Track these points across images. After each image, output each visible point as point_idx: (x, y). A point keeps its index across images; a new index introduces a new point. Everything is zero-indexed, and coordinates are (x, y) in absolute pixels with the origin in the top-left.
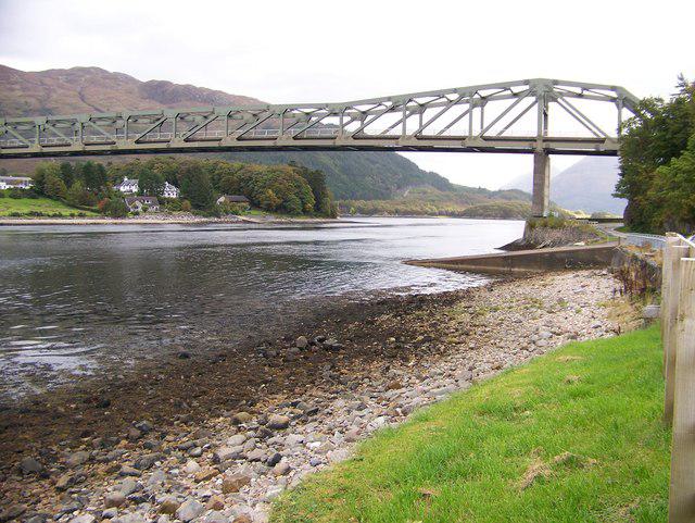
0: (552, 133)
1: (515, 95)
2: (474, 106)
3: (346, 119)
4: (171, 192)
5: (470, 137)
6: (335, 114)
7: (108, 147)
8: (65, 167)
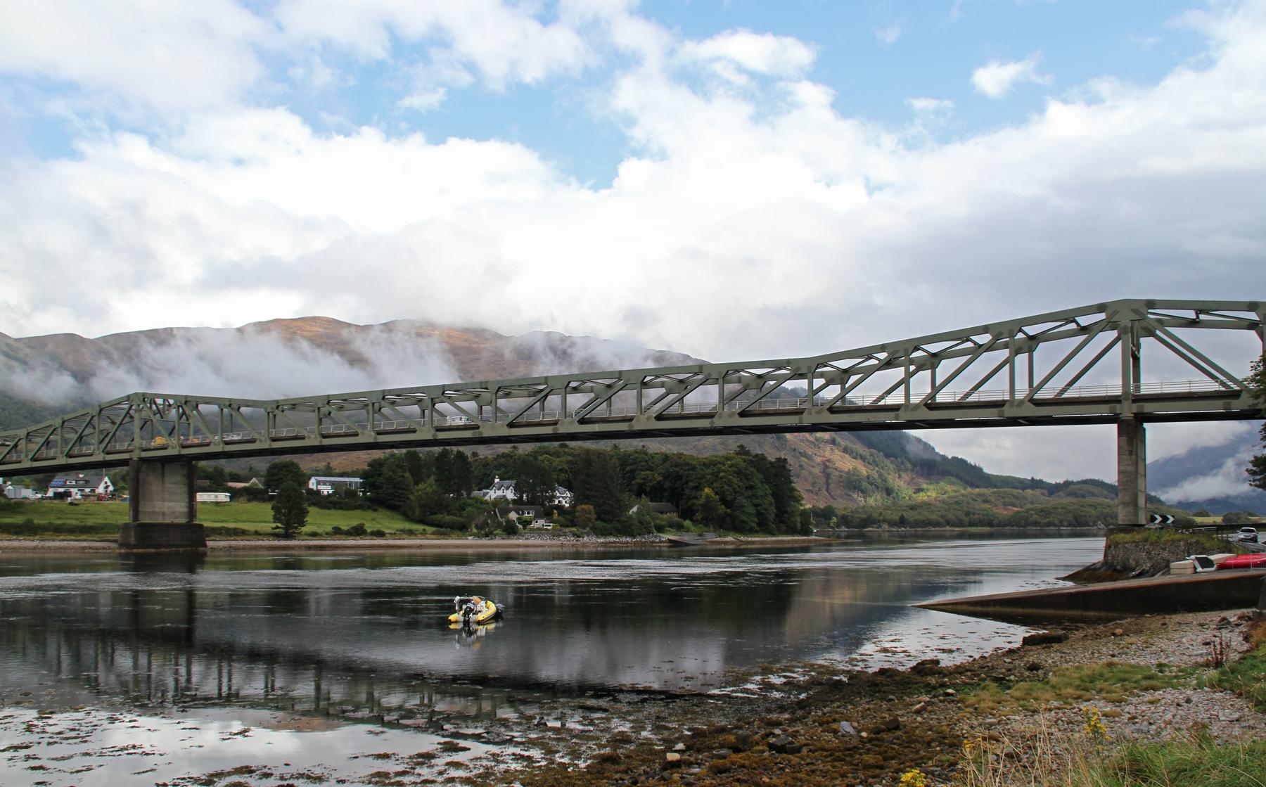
0: (1149, 384)
1: (1083, 330)
2: (1018, 351)
5: (1012, 402)
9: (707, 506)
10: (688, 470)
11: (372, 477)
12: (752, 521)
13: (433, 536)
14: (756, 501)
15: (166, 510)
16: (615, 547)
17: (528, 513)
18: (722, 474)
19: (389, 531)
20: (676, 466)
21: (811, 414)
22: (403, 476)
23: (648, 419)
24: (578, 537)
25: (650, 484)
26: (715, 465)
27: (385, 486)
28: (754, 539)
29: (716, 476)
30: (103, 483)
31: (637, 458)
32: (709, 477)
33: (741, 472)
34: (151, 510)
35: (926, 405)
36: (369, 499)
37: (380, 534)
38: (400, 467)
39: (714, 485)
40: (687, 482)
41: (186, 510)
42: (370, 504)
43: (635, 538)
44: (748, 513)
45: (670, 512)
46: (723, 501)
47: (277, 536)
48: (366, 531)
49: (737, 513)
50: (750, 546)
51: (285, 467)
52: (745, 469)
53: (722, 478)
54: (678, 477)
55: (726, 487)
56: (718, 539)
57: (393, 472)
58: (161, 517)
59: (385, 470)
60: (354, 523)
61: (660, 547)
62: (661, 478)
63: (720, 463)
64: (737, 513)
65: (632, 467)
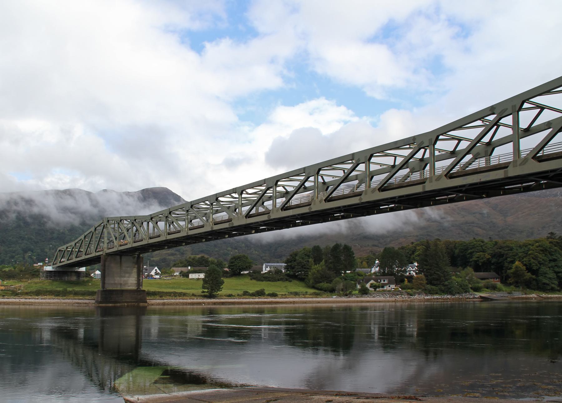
9: (517, 274)
10: (508, 250)
11: (291, 262)
12: (552, 283)
13: (311, 296)
14: (557, 269)
15: (122, 282)
16: (437, 302)
17: (384, 281)
18: (529, 252)
19: (281, 293)
20: (500, 249)
21: (432, 182)
22: (308, 261)
23: (320, 202)
24: (411, 295)
25: (482, 261)
26: (526, 246)
27: (296, 267)
28: (552, 296)
29: (526, 254)
30: (154, 270)
31: (475, 244)
32: (520, 254)
33: (546, 250)
34: (112, 282)
35: (534, 157)
36: (288, 275)
37: (274, 295)
38: (309, 256)
39: (524, 259)
40: (506, 259)
41: (136, 282)
42: (288, 278)
43: (454, 295)
44: (550, 278)
45: (494, 278)
46: (529, 269)
47: (205, 297)
48: (265, 293)
49: (540, 278)
50: (550, 300)
51: (239, 258)
52: (550, 248)
53: (530, 254)
54: (501, 255)
55: (532, 260)
56: (524, 296)
57: (303, 258)
58: (119, 286)
59: (297, 258)
60: (258, 289)
61: (474, 301)
62: (490, 257)
63: (530, 244)
64: (540, 278)
65: (472, 251)
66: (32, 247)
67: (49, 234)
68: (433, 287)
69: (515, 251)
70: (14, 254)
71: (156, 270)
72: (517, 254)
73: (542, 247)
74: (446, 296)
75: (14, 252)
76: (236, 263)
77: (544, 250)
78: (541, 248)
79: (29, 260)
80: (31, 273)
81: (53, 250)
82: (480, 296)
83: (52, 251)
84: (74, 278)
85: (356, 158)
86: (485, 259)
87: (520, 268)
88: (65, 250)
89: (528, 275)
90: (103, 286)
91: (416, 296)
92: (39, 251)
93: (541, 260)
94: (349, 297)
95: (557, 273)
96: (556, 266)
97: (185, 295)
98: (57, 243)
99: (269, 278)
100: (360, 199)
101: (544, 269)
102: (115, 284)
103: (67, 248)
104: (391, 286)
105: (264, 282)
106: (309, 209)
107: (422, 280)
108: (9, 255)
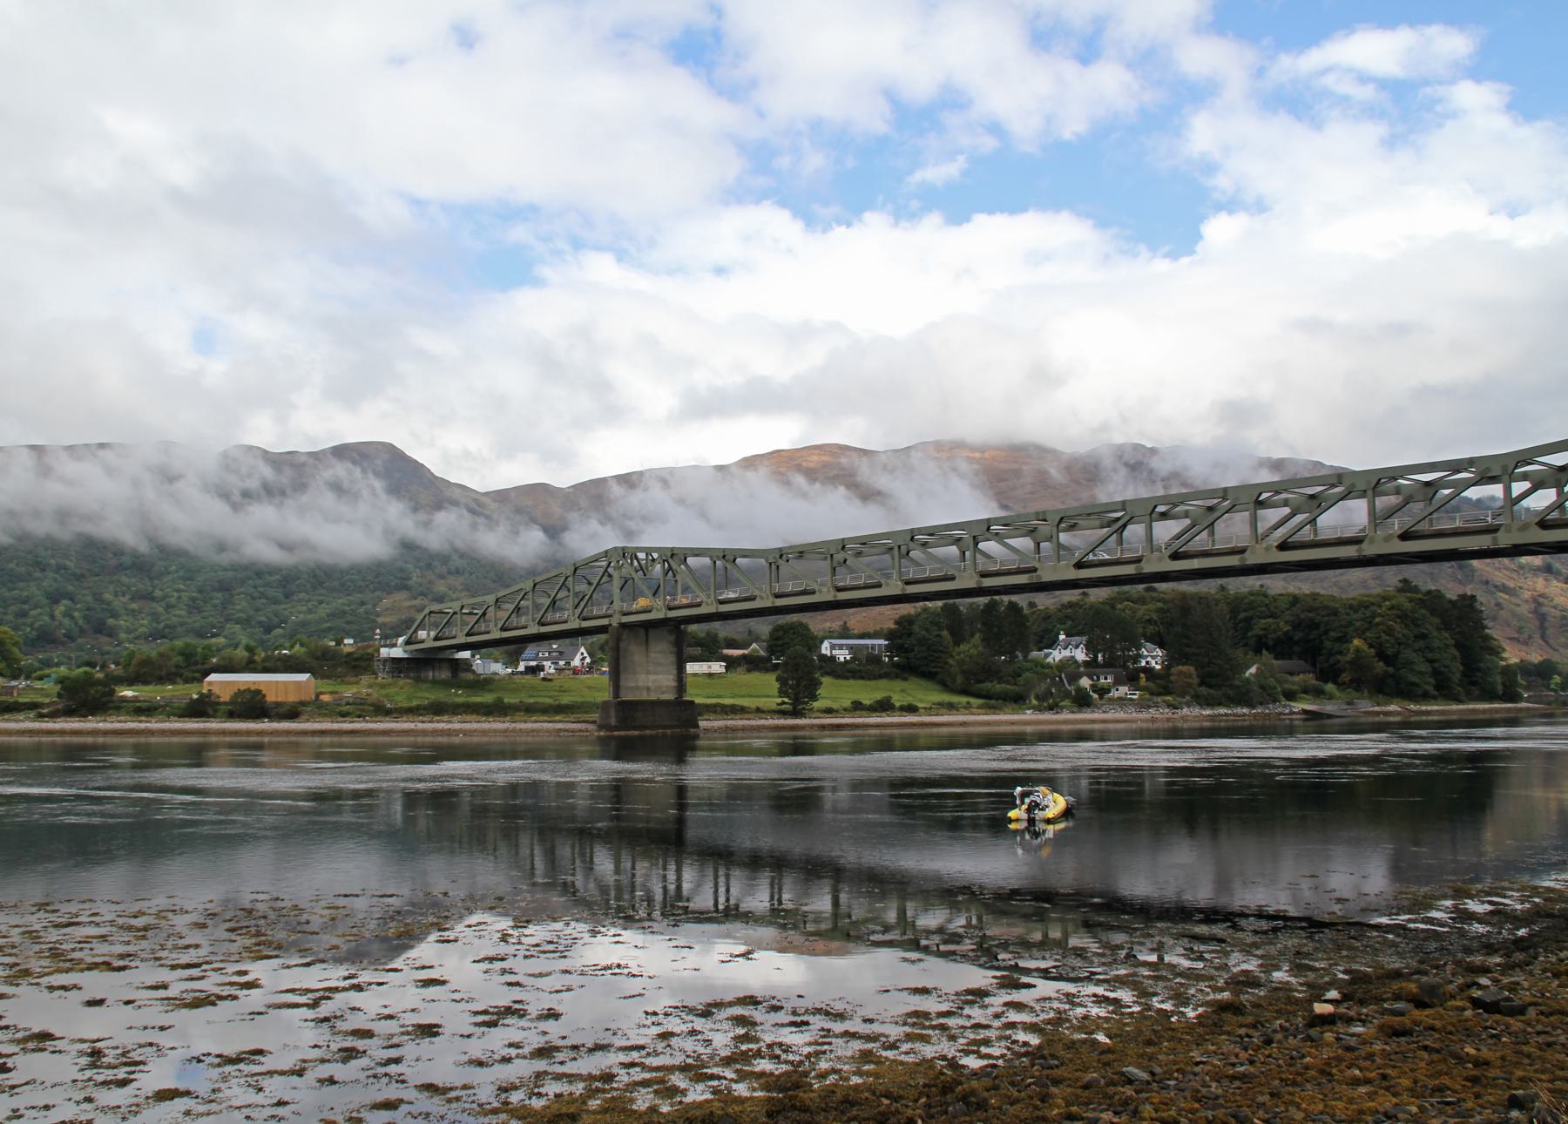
3: (1518, 488)
4: (1153, 657)
6: (1493, 480)
7: (1022, 579)
8: (951, 611)
9: (1358, 663)
10: (1328, 615)
11: (900, 638)
17: (1106, 679)
26: (1367, 607)
27: (916, 649)
28: (1429, 708)
29: (1370, 623)
31: (1253, 601)
32: (1358, 624)
34: (633, 685)
37: (911, 709)
40: (1327, 632)
41: (674, 684)
43: (1254, 708)
45: (1304, 673)
46: (1382, 656)
47: (783, 713)
49: (1402, 672)
51: (792, 629)
53: (1378, 624)
54: (1314, 625)
55: (1384, 637)
57: (927, 630)
58: (645, 693)
59: (916, 628)
60: (879, 696)
61: (1291, 720)
62: (1290, 628)
64: (1402, 672)
66: (71, 588)
67: (110, 555)
68: (1211, 691)
69: (1345, 616)
70: (25, 607)
71: (582, 654)
72: (1350, 623)
73: (1398, 609)
74: (1239, 710)
75: (25, 602)
76: (786, 640)
77: (1403, 617)
78: (1398, 612)
79: (66, 621)
80: (346, 662)
81: (124, 596)
82: (1303, 710)
83: (122, 599)
84: (445, 674)
85: (1347, 482)
86: (1279, 633)
87: (1364, 651)
88: (455, 613)
89: (1380, 667)
90: (616, 693)
91: (1185, 710)
92: (89, 598)
93: (1400, 636)
94: (1057, 713)
95: (1431, 661)
96: (1427, 647)
97: (742, 710)
98: (133, 580)
99: (860, 671)
100: (1359, 550)
101: (1408, 654)
102: (637, 688)
103: (462, 607)
104: (1120, 688)
105: (851, 682)
106: (1240, 560)
107: (1190, 676)
108: (13, 608)
